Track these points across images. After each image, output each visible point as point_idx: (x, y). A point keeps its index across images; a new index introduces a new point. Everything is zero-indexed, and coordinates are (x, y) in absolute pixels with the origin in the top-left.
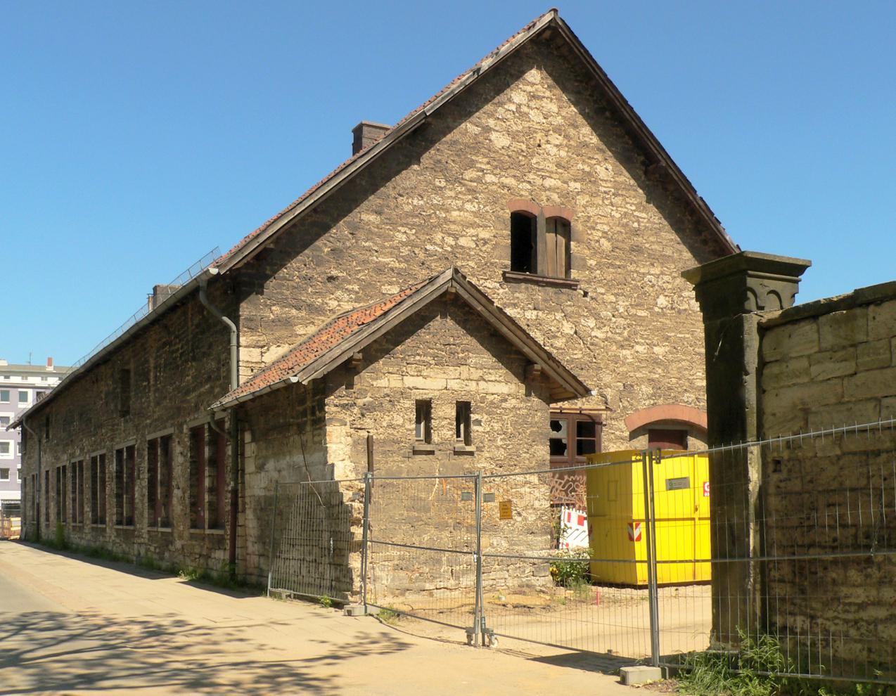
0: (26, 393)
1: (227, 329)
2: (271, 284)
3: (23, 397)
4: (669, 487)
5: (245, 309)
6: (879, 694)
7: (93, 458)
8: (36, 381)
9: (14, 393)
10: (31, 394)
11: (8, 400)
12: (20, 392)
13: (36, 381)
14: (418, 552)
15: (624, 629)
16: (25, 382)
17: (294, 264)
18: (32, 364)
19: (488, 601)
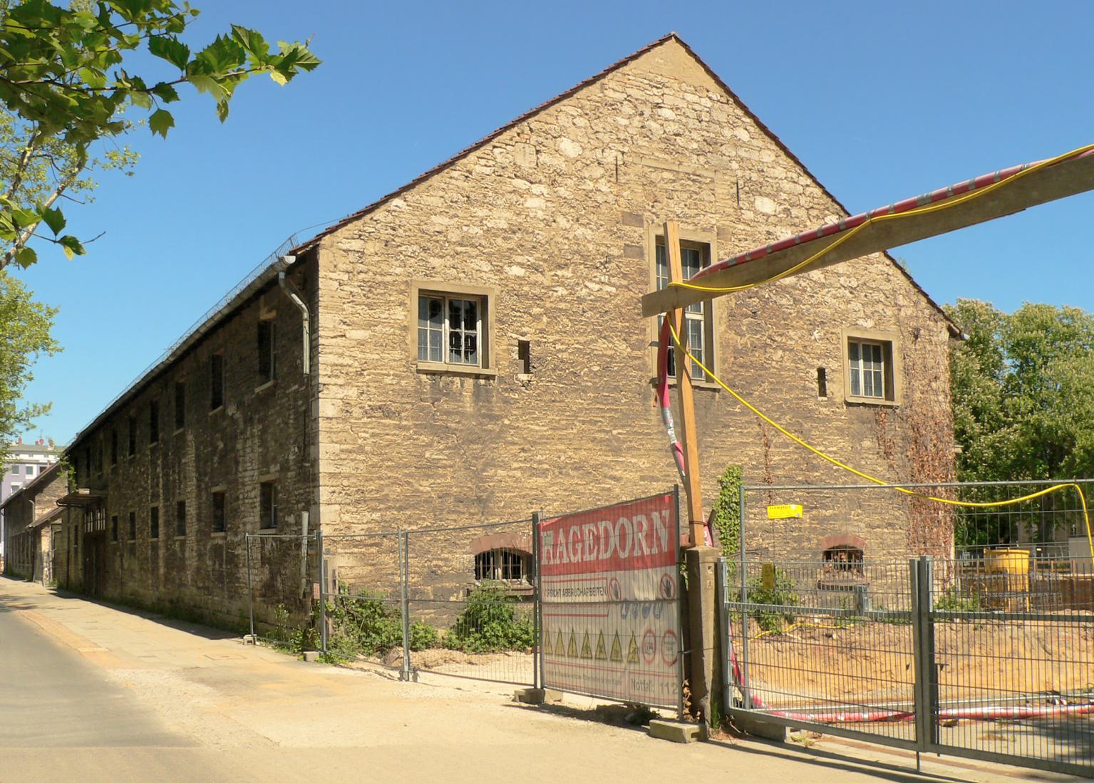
0: (32, 468)
1: (31, 504)
2: (45, 490)
3: (30, 471)
4: (76, 573)
5: (37, 498)
6: (1093, 763)
7: (215, 494)
8: (41, 458)
9: (22, 468)
10: (36, 469)
11: (17, 473)
12: (27, 467)
13: (41, 458)
14: (411, 555)
15: (877, 648)
16: (31, 458)
17: (53, 483)
18: (50, 329)
19: (572, 556)
